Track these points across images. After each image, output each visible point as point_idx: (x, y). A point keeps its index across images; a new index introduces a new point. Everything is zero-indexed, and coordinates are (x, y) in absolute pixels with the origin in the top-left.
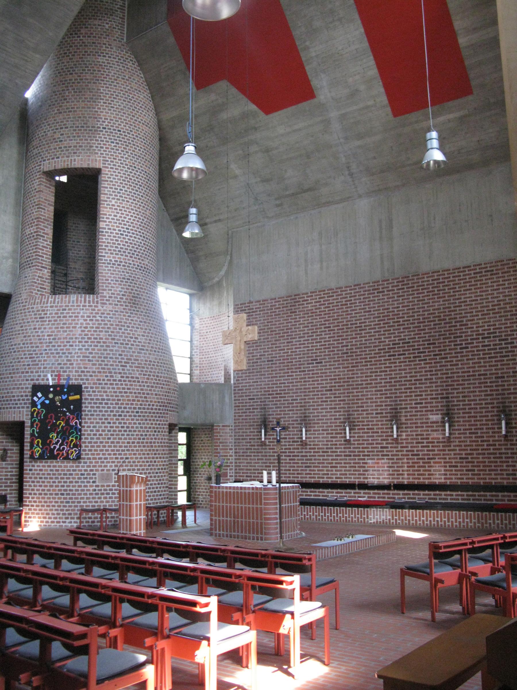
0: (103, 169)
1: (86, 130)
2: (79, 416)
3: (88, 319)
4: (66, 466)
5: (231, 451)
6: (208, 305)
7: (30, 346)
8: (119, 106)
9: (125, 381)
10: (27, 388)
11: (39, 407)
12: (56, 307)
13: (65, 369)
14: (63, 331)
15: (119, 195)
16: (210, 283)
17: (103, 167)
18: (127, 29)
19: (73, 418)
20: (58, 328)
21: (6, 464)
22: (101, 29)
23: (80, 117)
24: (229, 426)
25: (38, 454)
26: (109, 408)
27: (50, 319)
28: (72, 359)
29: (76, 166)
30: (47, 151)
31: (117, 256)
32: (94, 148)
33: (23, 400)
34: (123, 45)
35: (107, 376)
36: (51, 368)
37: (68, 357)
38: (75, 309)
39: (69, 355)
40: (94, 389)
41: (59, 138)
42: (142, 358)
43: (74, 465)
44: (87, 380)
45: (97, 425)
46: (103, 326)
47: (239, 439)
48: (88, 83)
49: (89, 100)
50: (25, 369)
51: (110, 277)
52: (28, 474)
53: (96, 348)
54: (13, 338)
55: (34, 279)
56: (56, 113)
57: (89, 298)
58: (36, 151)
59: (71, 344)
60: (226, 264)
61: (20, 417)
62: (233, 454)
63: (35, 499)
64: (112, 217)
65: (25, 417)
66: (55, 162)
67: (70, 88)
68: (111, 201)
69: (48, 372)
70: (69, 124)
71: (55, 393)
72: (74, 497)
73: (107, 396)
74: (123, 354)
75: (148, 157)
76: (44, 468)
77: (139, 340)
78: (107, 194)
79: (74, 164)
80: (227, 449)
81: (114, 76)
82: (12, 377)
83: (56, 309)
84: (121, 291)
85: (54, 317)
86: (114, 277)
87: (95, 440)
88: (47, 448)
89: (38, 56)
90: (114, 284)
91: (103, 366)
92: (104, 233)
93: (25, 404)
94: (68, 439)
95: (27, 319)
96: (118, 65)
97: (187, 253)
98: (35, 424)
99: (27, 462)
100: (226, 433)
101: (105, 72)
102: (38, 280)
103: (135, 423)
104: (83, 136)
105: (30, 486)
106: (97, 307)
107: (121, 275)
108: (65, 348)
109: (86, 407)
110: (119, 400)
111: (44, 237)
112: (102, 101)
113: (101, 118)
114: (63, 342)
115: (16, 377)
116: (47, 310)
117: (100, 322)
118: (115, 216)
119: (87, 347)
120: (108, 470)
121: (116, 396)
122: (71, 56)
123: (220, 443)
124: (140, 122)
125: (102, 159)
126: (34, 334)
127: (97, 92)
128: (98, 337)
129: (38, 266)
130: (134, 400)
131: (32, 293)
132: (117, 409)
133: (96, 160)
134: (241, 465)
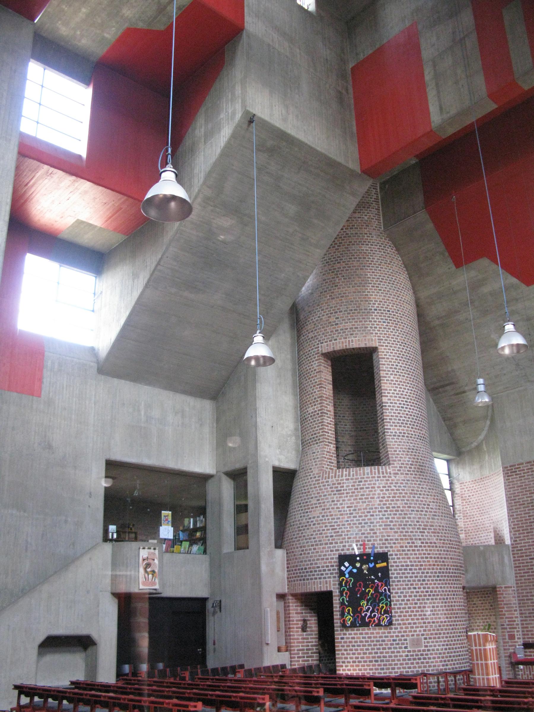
0: (379, 347)
1: (359, 313)
2: (387, 584)
3: (384, 489)
4: (373, 633)
5: (516, 613)
6: (468, 469)
7: (330, 518)
8: (386, 288)
9: (425, 547)
10: (332, 558)
11: (347, 576)
12: (352, 479)
13: (369, 539)
14: (362, 502)
15: (396, 370)
16: (468, 449)
17: (379, 345)
18: (383, 219)
19: (382, 585)
20: (356, 499)
21: (306, 635)
22: (361, 221)
23: (352, 301)
24: (511, 587)
25: (349, 623)
26: (413, 573)
27: (348, 491)
28: (375, 528)
29: (355, 346)
30: (323, 334)
31: (401, 428)
32: (369, 329)
33: (329, 570)
34: (381, 233)
35: (409, 543)
36: (356, 538)
37: (370, 526)
38: (370, 481)
39: (372, 525)
40: (398, 556)
41: (335, 321)
42: (436, 524)
43: (386, 631)
44: (391, 547)
45: (404, 591)
46: (398, 495)
47: (524, 600)
48: (356, 269)
49: (358, 285)
50: (329, 540)
51: (398, 448)
52: (341, 642)
53: (395, 516)
54: (310, 512)
55: (324, 454)
56: (328, 299)
57: (382, 469)
58: (311, 335)
59: (371, 513)
60: (486, 428)
61: (327, 587)
62: (518, 615)
63: (349, 668)
64: (393, 391)
65: (332, 586)
66: (333, 344)
67: (340, 276)
68: (389, 377)
69: (353, 542)
70: (343, 308)
71: (362, 562)
72: (388, 663)
73: (411, 562)
74: (420, 520)
75: (414, 333)
76: (356, 636)
77: (431, 506)
78: (385, 371)
79: (352, 345)
80: (511, 611)
81: (378, 262)
82: (315, 549)
83: (352, 481)
84: (409, 461)
85: (351, 489)
86: (401, 448)
87: (403, 606)
88: (358, 616)
89: (318, 250)
90: (402, 454)
91: (404, 534)
92: (387, 407)
93: (331, 574)
94: (379, 606)
95: (323, 492)
96: (379, 251)
97: (444, 421)
98: (344, 593)
99: (337, 631)
100: (509, 594)
101: (370, 258)
102: (327, 455)
103: (437, 588)
104: (357, 319)
105: (343, 654)
106: (391, 477)
107: (407, 446)
108: (366, 518)
109: (392, 574)
110: (421, 565)
111: (327, 414)
112: (370, 285)
113: (372, 301)
114: (364, 513)
115: (319, 548)
116: (343, 483)
117: (395, 491)
118: (395, 390)
119: (387, 516)
120: (418, 635)
121: (419, 562)
122: (336, 247)
123: (505, 604)
124: (404, 301)
125: (377, 338)
126: (333, 506)
127: (365, 278)
128: (396, 506)
129: (326, 442)
130: (434, 565)
131: (323, 467)
132: (421, 574)
133: (372, 340)
134: (529, 626)
